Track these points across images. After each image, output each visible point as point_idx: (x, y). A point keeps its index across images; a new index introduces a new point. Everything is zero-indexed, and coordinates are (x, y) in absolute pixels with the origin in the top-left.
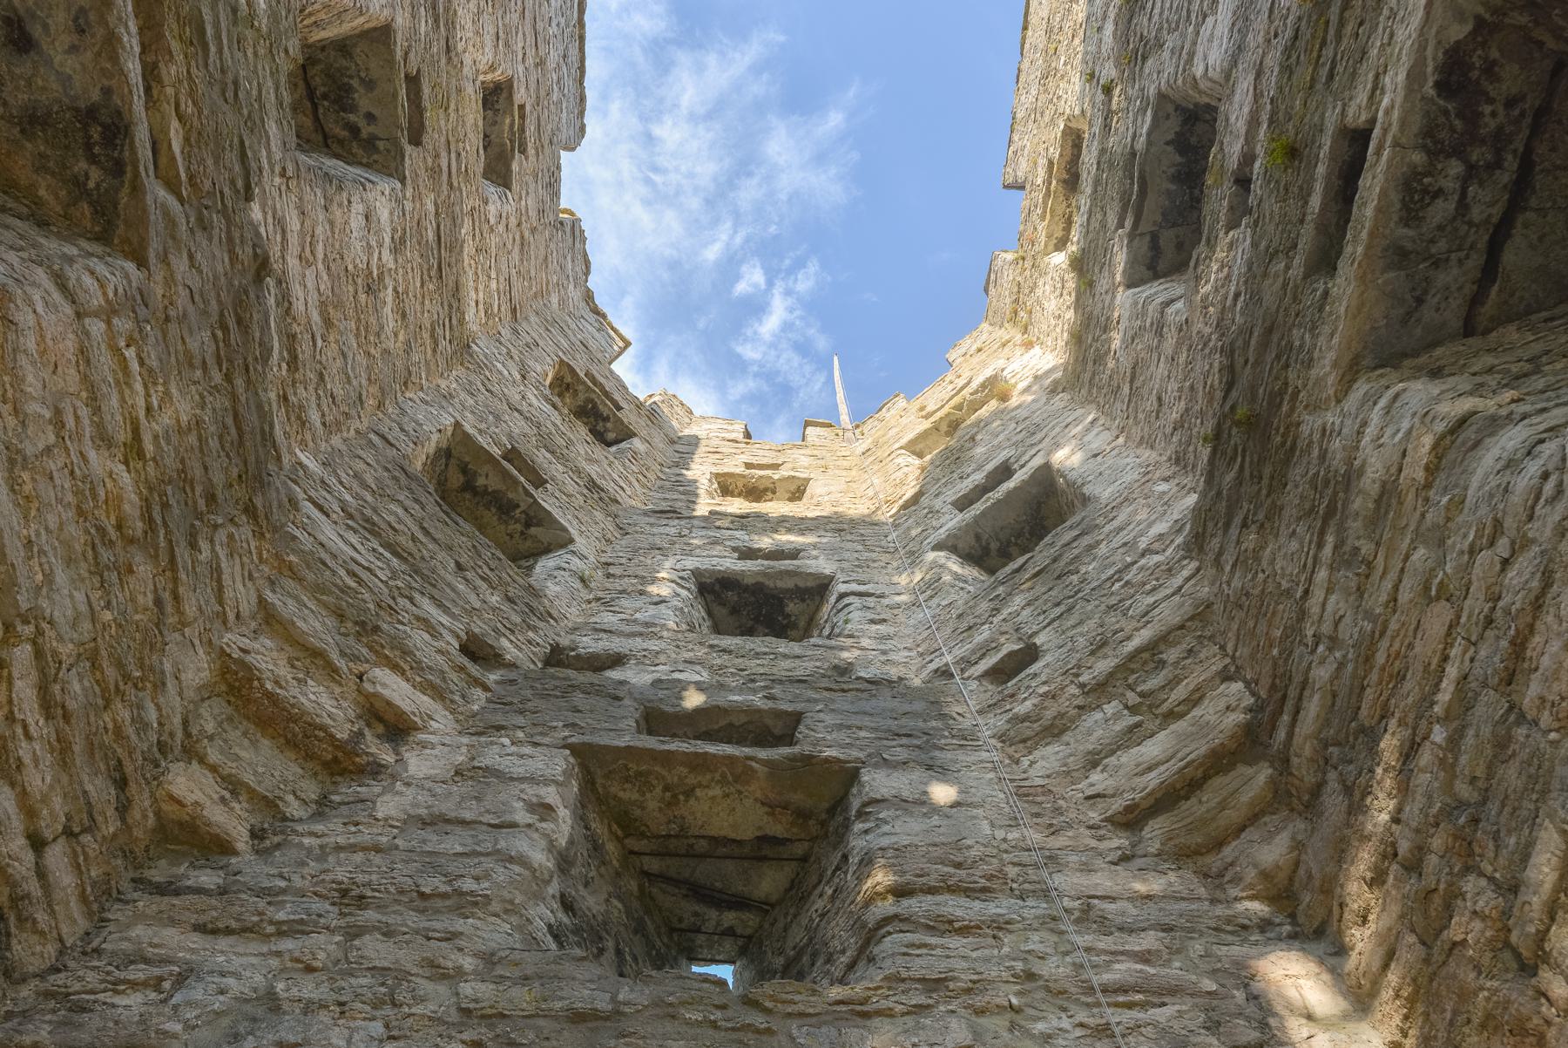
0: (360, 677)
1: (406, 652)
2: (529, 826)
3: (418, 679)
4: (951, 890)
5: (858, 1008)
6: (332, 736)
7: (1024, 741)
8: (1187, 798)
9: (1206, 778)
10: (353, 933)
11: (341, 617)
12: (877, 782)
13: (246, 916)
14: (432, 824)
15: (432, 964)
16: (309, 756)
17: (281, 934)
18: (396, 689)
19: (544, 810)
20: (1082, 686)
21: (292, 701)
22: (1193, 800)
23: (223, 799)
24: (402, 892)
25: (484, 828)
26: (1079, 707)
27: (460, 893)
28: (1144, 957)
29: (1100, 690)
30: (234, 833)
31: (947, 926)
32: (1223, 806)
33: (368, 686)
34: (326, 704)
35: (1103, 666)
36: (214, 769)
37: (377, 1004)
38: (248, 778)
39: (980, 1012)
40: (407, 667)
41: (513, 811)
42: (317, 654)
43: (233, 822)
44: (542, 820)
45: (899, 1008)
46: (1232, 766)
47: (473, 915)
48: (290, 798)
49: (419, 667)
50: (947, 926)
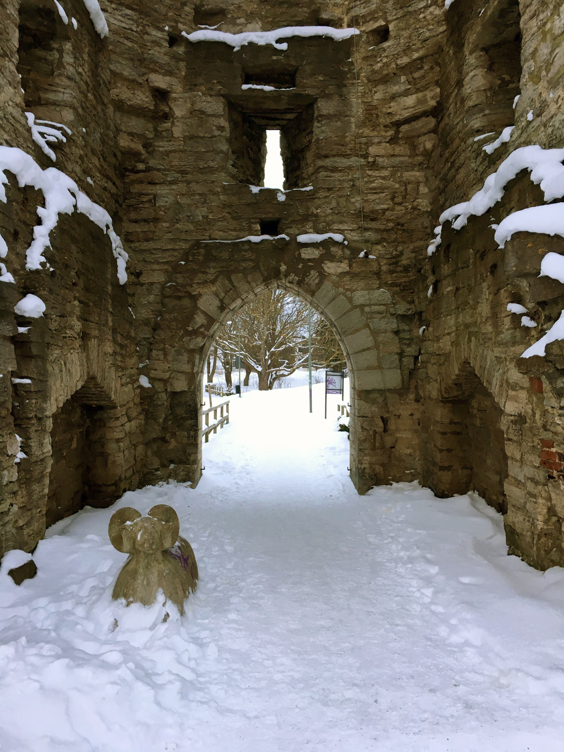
0: (147, 80)
1: (156, 63)
2: (219, 135)
3: (163, 71)
4: (339, 155)
5: (312, 197)
6: (150, 109)
7: (375, 81)
8: (414, 121)
9: (421, 117)
10: (188, 183)
11: (132, 60)
12: (325, 107)
13: (160, 179)
14: (192, 138)
15: (211, 191)
16: (145, 116)
17: (171, 184)
18: (159, 81)
19: (221, 129)
20: (397, 65)
21: (136, 104)
22: (416, 122)
23: (131, 140)
24: (195, 168)
25: (207, 139)
26: (395, 74)
27: (209, 167)
28: (384, 178)
29: (403, 69)
30: (139, 149)
31: (335, 170)
32: (422, 127)
33: (151, 84)
34: (142, 98)
35: (405, 60)
36: (125, 132)
37: (203, 203)
38: (135, 131)
39: (340, 197)
40: (158, 69)
41: (212, 131)
42: (133, 81)
43: (138, 146)
44: (222, 132)
45: (321, 197)
46: (428, 116)
47: (215, 174)
48: (147, 132)
49: (161, 66)
50: (335, 170)
